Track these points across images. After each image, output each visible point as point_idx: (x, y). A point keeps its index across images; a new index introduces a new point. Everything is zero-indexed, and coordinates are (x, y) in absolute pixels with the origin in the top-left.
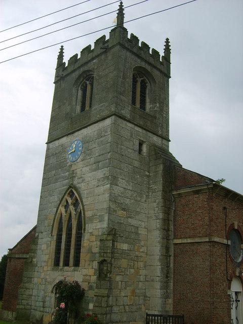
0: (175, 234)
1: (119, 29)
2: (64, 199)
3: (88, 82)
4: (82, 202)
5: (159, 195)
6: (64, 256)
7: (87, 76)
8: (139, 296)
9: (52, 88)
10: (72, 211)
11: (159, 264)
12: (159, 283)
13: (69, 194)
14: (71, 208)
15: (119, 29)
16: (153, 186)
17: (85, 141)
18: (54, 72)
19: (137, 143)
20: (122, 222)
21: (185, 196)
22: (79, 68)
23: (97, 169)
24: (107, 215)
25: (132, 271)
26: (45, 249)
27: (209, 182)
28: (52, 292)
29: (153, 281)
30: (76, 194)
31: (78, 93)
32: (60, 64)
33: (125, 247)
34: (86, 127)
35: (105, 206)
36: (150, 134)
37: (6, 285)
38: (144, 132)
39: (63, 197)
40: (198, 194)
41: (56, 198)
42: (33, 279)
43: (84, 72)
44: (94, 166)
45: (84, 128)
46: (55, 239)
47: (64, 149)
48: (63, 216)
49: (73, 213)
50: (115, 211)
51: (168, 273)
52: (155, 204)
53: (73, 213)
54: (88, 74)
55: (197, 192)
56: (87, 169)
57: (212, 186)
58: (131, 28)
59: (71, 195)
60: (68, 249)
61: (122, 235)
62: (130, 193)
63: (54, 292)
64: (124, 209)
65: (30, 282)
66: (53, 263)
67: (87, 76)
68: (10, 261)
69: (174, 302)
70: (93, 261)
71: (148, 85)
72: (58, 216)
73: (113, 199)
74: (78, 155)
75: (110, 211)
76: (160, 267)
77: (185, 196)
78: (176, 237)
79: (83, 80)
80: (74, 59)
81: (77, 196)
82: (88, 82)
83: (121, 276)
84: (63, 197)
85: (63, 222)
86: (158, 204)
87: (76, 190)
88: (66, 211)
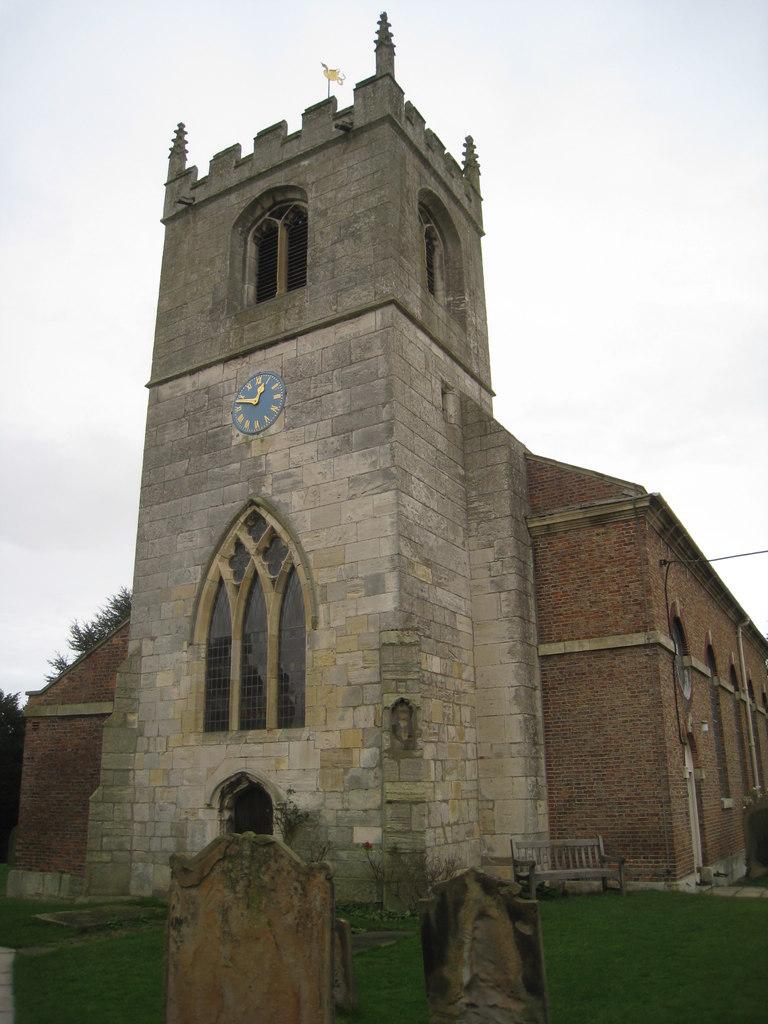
0: (540, 630)
1: (381, 86)
2: (230, 539)
3: (279, 223)
4: (298, 543)
5: (504, 529)
6: (242, 701)
7: (275, 204)
8: (468, 799)
9: (156, 236)
10: (261, 571)
11: (516, 709)
12: (521, 760)
13: (246, 522)
14: (258, 563)
15: (381, 86)
16: (482, 506)
17: (292, 376)
18: (160, 193)
19: (438, 387)
20: (426, 595)
21: (566, 532)
22: (251, 180)
23: (346, 447)
24: (395, 573)
25: (452, 730)
26: (171, 678)
27: (632, 493)
28: (209, 806)
29: (499, 755)
30: (270, 520)
31: (246, 248)
32: (179, 173)
33: (435, 664)
34: (294, 337)
35: (387, 549)
36: (459, 370)
37: (25, 800)
38: (448, 359)
39: (227, 531)
40: (604, 525)
41: (194, 541)
42: (131, 774)
43: (270, 192)
44: (335, 442)
45: (286, 339)
46: (203, 655)
47: (214, 398)
48: (229, 589)
49: (265, 575)
50: (411, 564)
51: (535, 734)
52: (490, 554)
53: (265, 575)
54: (279, 199)
55: (598, 521)
56: (310, 450)
57: (647, 504)
58: (414, 83)
59: (255, 523)
60: (250, 684)
61: (428, 633)
62: (436, 519)
63: (216, 804)
64: (427, 563)
65: (125, 783)
66: (201, 722)
67: (275, 204)
68: (36, 727)
69: (552, 808)
70: (355, 708)
71: (438, 243)
72: (210, 587)
73: (405, 531)
74: (270, 414)
75: (401, 566)
76: (520, 717)
77: (566, 532)
78: (542, 641)
79: (263, 214)
80: (227, 158)
81: (278, 528)
82: (279, 223)
83: (433, 745)
84: (227, 531)
85: (230, 600)
86: (501, 551)
87: (273, 510)
88: (238, 574)
